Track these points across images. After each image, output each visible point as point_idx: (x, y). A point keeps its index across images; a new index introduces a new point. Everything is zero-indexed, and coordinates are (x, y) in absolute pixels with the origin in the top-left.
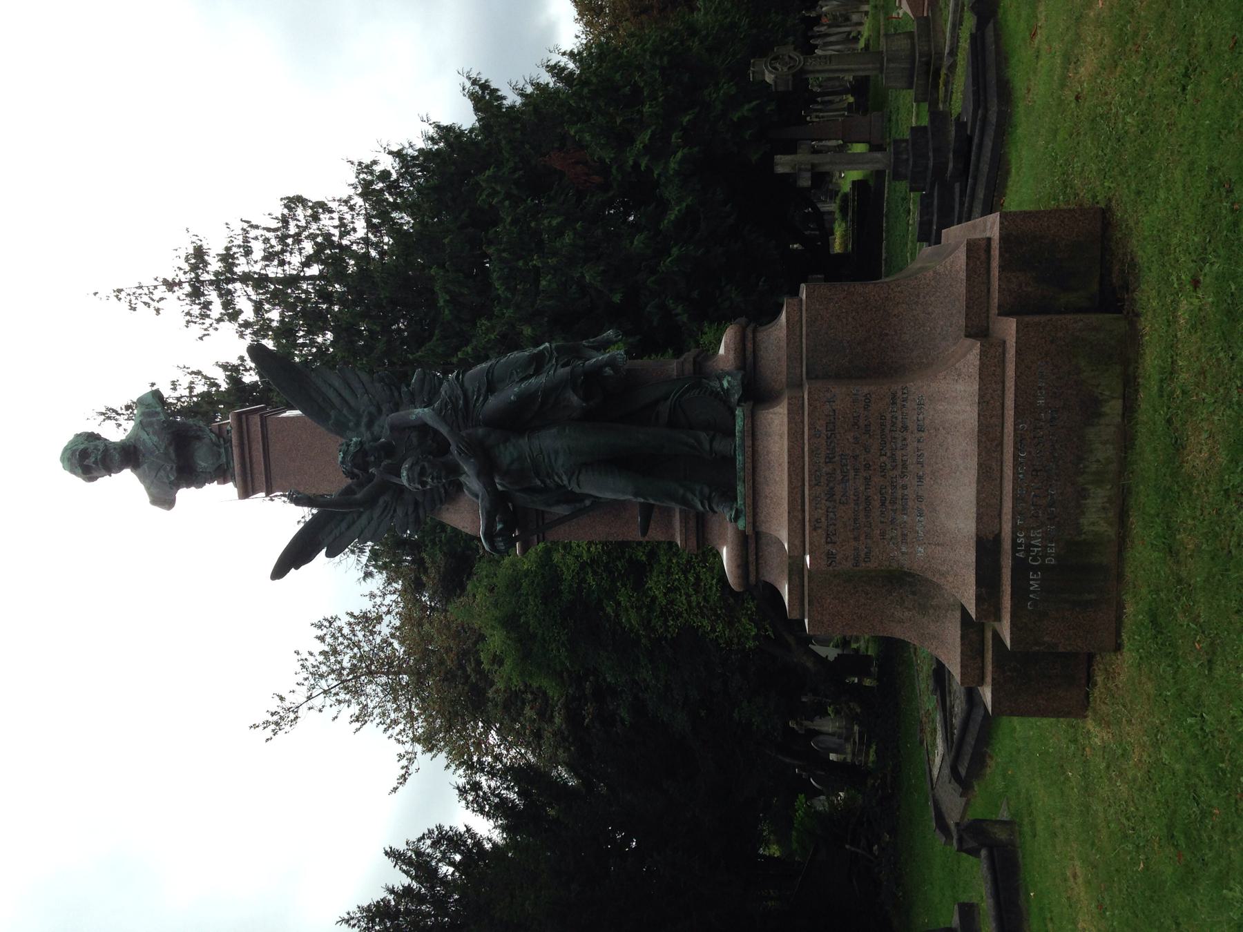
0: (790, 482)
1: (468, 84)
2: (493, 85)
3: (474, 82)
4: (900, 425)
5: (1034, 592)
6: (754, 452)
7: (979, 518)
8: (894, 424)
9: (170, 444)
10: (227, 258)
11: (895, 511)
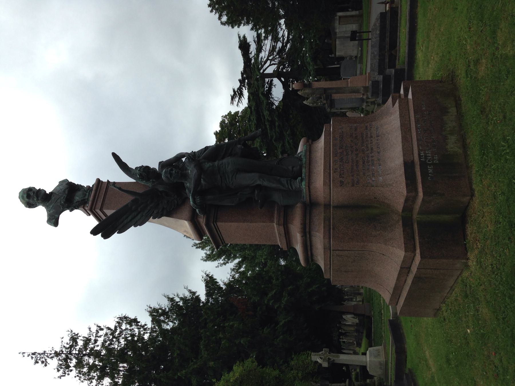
0: (325, 159)
1: (205, 275)
2: (215, 277)
3: (207, 275)
4: (369, 136)
5: (430, 173)
6: (310, 157)
7: (404, 155)
8: (367, 136)
9: (67, 188)
10: (87, 341)
11: (369, 165)
